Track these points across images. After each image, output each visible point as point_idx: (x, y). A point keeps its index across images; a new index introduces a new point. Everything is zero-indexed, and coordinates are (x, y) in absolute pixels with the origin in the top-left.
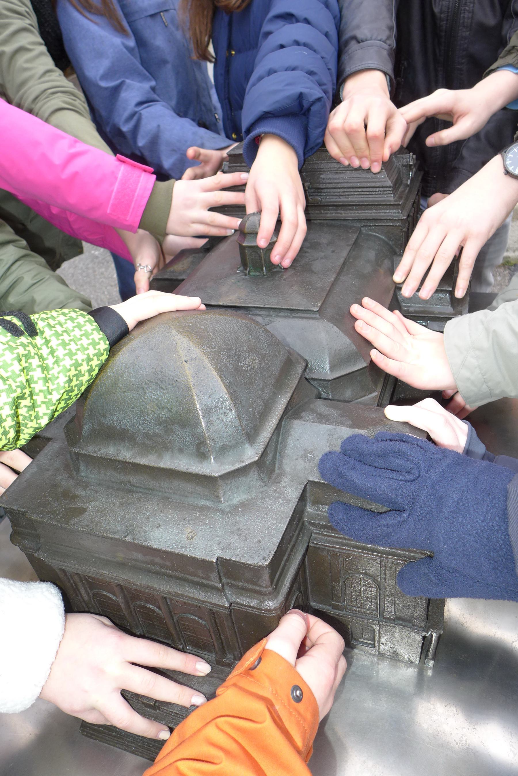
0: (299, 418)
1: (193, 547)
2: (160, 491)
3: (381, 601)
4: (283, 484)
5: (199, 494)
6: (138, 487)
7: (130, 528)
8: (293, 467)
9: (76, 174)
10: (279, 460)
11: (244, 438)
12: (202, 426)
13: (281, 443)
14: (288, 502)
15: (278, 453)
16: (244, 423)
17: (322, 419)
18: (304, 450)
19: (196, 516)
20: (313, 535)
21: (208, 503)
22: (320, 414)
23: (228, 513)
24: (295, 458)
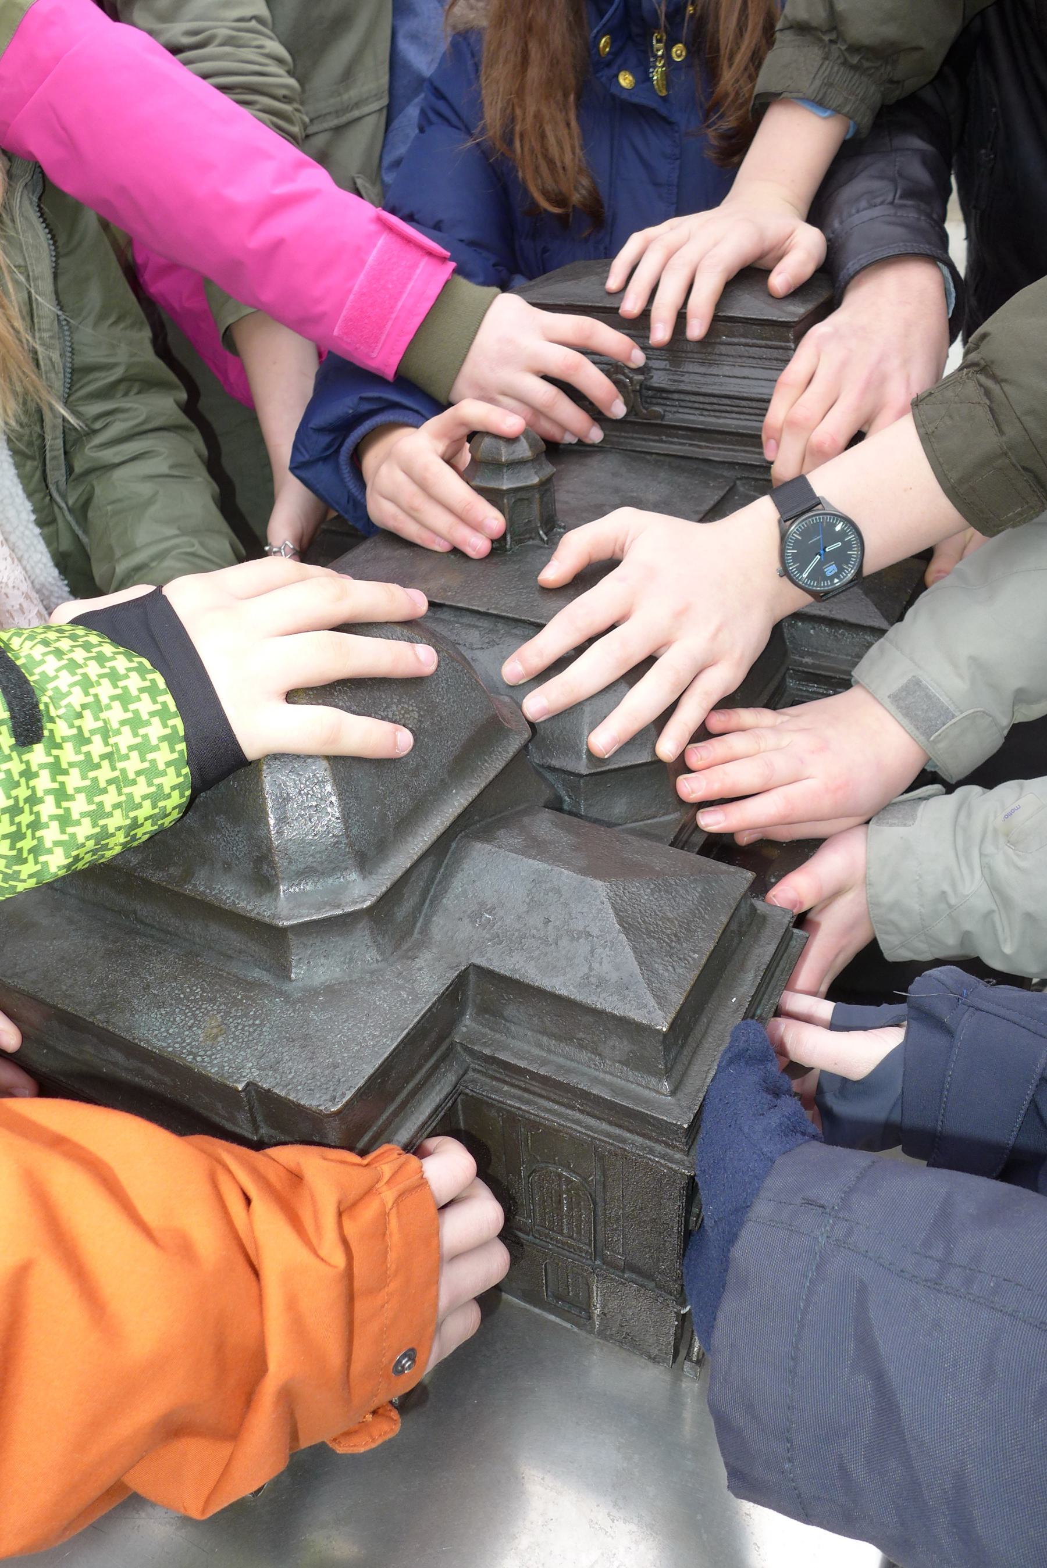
0: (488, 841)
1: (210, 1056)
2: (185, 940)
3: (598, 1228)
4: (420, 962)
5: (253, 956)
6: (149, 925)
7: (108, 1000)
8: (450, 934)
9: (278, 244)
10: (426, 916)
11: (350, 862)
12: (267, 824)
13: (440, 882)
14: (416, 998)
15: (428, 902)
16: (355, 831)
17: (536, 848)
18: (479, 904)
19: (235, 998)
20: (470, 1074)
21: (265, 977)
22: (534, 839)
23: (299, 1001)
24: (457, 916)
